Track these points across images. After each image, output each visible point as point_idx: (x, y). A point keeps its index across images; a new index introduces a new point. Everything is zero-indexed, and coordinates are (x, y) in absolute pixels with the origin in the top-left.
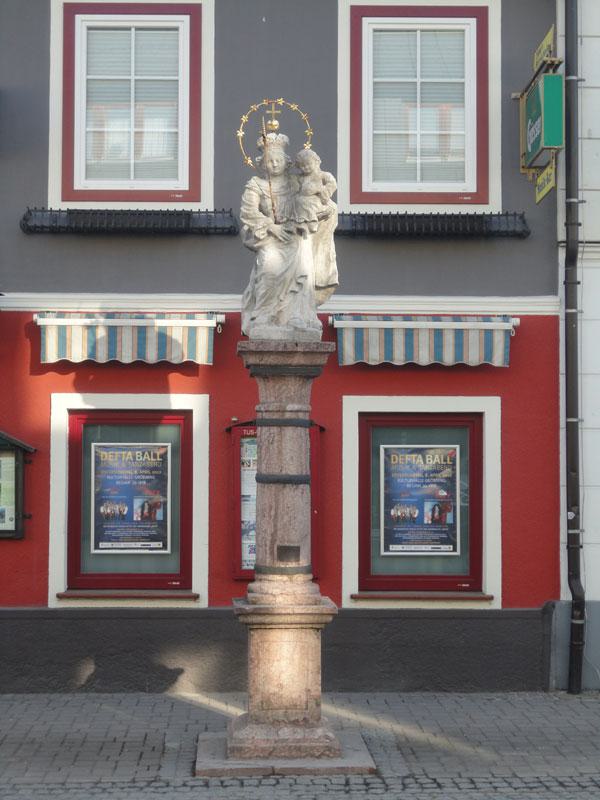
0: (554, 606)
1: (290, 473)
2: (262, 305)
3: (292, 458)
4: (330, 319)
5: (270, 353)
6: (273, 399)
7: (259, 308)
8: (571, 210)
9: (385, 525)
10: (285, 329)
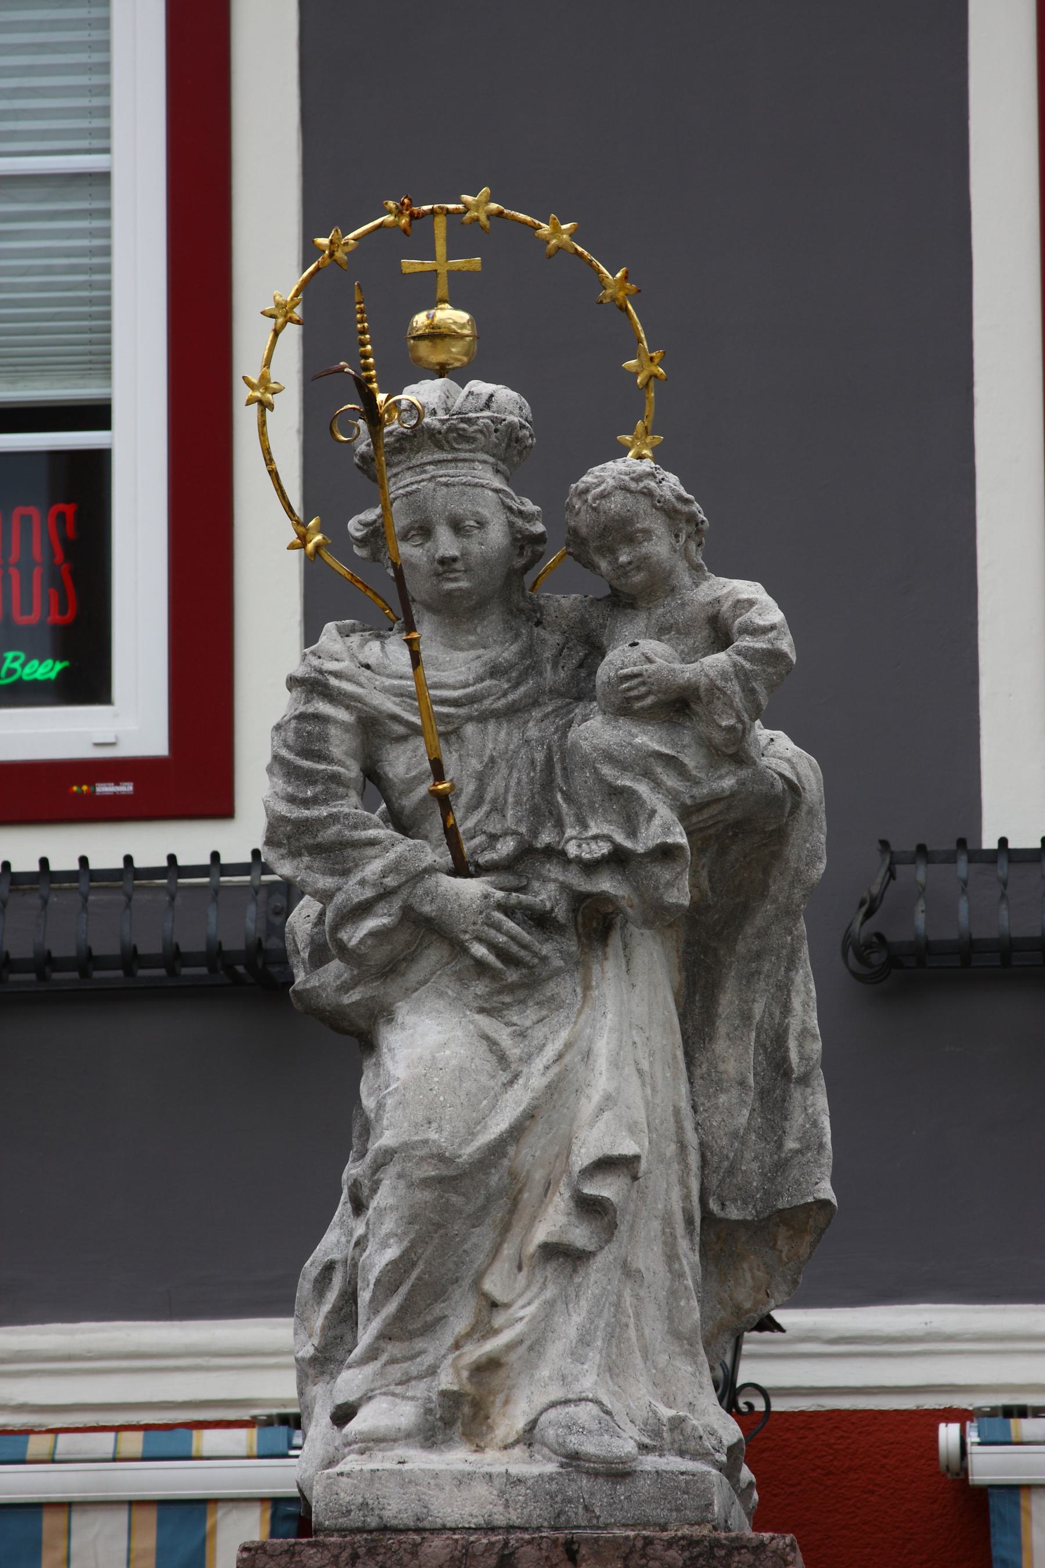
9: (319, 211)
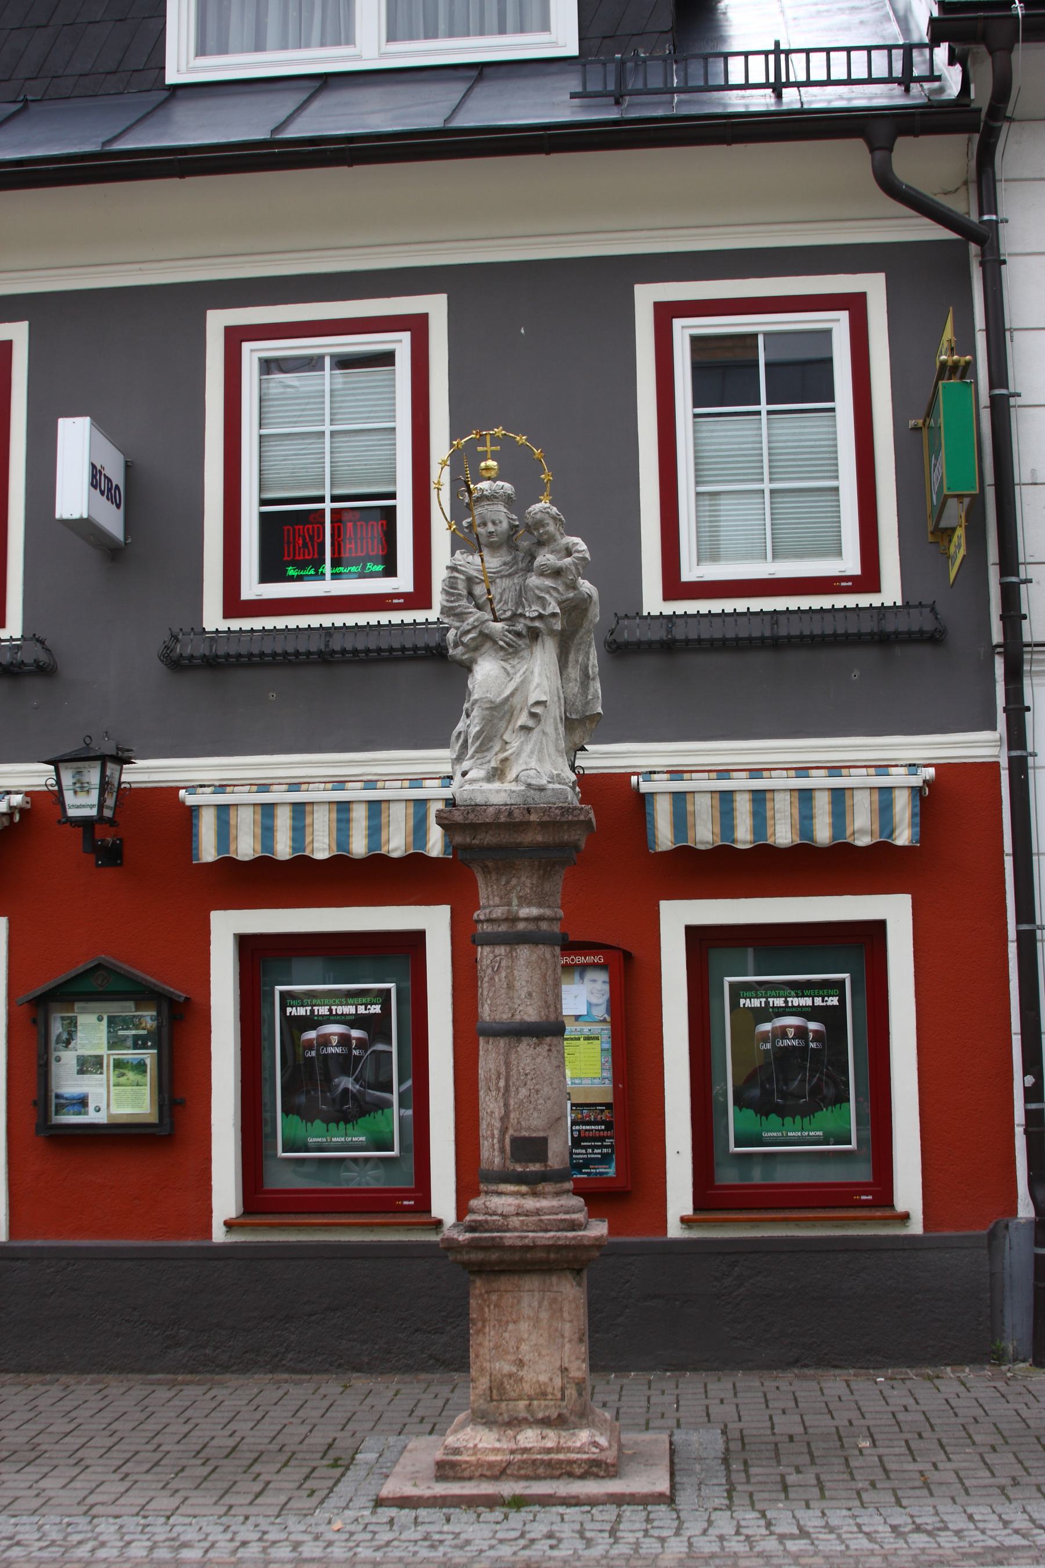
0: (1007, 1227)
1: (527, 1019)
2: (476, 752)
3: (530, 994)
4: (634, 779)
5: (486, 826)
6: (497, 900)
7: (472, 757)
8: (1011, 596)
10: (514, 787)
